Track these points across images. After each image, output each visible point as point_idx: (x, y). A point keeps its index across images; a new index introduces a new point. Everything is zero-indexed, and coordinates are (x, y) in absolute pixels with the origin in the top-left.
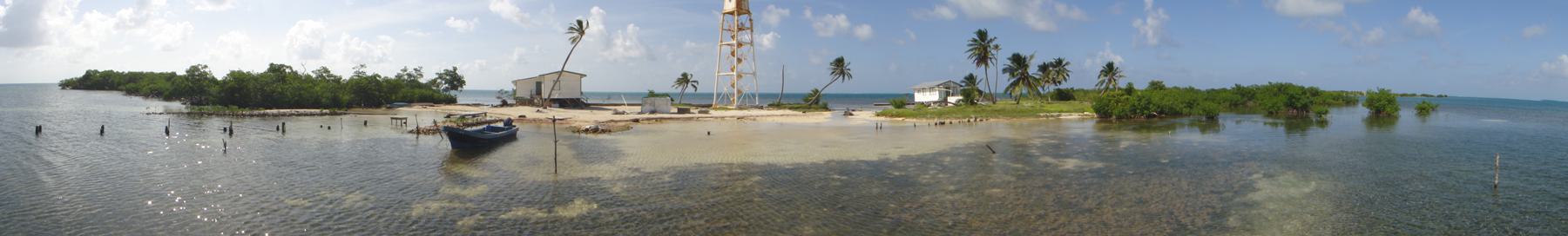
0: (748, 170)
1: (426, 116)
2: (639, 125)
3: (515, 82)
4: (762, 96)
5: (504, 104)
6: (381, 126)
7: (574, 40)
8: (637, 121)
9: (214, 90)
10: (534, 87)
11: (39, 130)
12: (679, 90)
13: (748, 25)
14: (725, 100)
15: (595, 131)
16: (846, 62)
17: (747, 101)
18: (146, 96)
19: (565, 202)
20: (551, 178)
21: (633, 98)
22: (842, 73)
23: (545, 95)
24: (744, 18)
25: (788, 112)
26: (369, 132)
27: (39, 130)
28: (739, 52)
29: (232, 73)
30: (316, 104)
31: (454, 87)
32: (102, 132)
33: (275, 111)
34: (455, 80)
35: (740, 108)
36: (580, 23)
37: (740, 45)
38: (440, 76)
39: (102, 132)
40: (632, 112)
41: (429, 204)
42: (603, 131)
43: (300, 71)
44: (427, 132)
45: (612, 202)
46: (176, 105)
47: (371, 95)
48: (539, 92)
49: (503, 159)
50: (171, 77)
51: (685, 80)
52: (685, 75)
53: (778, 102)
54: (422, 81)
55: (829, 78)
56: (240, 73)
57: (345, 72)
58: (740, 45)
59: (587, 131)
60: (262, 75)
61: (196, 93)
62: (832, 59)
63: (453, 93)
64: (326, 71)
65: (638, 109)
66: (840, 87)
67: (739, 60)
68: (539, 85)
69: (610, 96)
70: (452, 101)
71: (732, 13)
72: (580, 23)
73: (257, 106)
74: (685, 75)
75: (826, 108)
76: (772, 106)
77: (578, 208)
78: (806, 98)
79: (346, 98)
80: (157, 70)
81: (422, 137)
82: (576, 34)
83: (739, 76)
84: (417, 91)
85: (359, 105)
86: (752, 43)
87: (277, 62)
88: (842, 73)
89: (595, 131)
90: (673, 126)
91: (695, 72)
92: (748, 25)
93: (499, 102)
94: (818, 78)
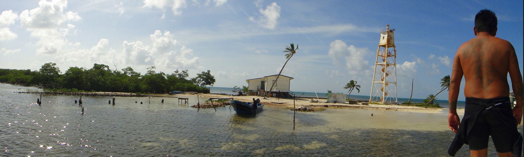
0: (402, 133)
1: (193, 99)
2: (328, 109)
3: (248, 81)
4: (399, 100)
5: (240, 94)
6: (172, 102)
7: (288, 57)
8: (327, 106)
9: (61, 79)
10: (259, 84)
11: (372, 115)
13: (393, 53)
14: (377, 100)
15: (305, 110)
17: (390, 101)
18: (13, 83)
19: (309, 142)
20: (292, 131)
21: (322, 96)
23: (267, 88)
26: (165, 107)
27: (372, 115)
28: (387, 69)
29: (72, 69)
30: (126, 90)
31: (209, 83)
32: (292, 50)
33: (102, 93)
34: (209, 79)
35: (386, 104)
36: (292, 46)
37: (388, 65)
38: (200, 76)
39: (292, 50)
40: (323, 102)
42: (310, 110)
43: (112, 69)
44: (204, 107)
45: (332, 143)
46: (33, 89)
47: (158, 85)
48: (263, 87)
49: (261, 119)
50: (28, 72)
51: (352, 85)
53: (408, 102)
54: (188, 79)
56: (76, 68)
57: (142, 70)
58: (388, 65)
59: (299, 110)
60: (87, 72)
61: (47, 81)
62: (443, 77)
63: (208, 86)
64: (130, 69)
65: (326, 100)
67: (387, 75)
68: (263, 83)
69: (303, 94)
70: (207, 91)
71: (384, 46)
72: (292, 46)
73: (89, 90)
75: (438, 106)
76: (404, 104)
77: (315, 145)
78: (425, 101)
79: (144, 87)
80: (19, 69)
81: (201, 110)
82: (289, 53)
84: (186, 84)
85: (152, 92)
87: (99, 63)
89: (305, 110)
90: (346, 110)
91: (359, 81)
92: (393, 53)
93: (237, 93)
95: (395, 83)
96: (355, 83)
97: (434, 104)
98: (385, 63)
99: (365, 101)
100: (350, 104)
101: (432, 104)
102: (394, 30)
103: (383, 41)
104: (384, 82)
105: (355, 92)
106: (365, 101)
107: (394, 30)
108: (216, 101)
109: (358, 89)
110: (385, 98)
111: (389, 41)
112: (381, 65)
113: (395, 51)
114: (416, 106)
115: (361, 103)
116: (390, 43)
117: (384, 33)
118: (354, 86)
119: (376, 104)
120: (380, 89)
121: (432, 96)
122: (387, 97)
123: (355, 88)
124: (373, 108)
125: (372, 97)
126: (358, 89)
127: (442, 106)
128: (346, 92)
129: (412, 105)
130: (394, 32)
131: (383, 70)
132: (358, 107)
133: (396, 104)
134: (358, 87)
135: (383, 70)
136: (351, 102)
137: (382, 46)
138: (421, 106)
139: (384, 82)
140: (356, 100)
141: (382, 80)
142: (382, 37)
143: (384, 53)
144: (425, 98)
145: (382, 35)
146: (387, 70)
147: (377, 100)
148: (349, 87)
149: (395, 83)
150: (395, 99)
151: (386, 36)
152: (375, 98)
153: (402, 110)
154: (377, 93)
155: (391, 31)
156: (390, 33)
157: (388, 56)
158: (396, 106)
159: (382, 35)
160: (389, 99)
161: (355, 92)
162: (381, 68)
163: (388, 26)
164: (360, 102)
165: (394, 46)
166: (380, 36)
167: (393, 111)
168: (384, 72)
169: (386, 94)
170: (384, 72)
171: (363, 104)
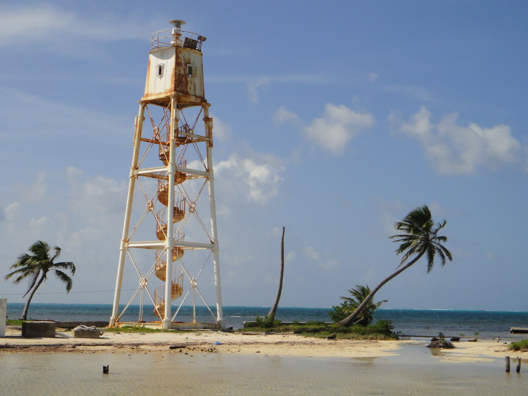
4: (228, 312)
11: (106, 370)
12: (252, 184)
13: (200, 130)
14: (140, 316)
16: (436, 218)
22: (428, 248)
24: (191, 115)
25: (300, 338)
27: (106, 370)
28: (180, 192)
37: (180, 176)
41: (248, 164)
51: (38, 260)
52: (40, 249)
53: (268, 322)
55: (396, 260)
62: (403, 214)
66: (415, 288)
67: (178, 213)
71: (163, 103)
74: (40, 249)
75: (387, 332)
78: (337, 314)
83: (177, 251)
86: (208, 173)
88: (428, 248)
91: (67, 246)
92: (200, 130)
94: (364, 257)
95: (213, 246)
96: (51, 254)
97: (374, 323)
98: (169, 169)
99: (93, 323)
100: (25, 336)
101: (364, 323)
102: (202, 39)
103: (160, 83)
104: (166, 243)
105: (51, 291)
106: (93, 323)
107: (202, 39)
108: (69, 347)
109: (65, 278)
110: (173, 310)
111: (181, 81)
112: (153, 176)
113: (207, 119)
114: (298, 332)
115: (71, 334)
116: (186, 90)
117: (162, 53)
118: (46, 266)
119: (136, 330)
120: (151, 272)
121: (363, 293)
122: (181, 302)
123: (51, 272)
124: (121, 346)
125: (120, 308)
126: (65, 278)
127: (404, 331)
128: (17, 292)
129: (284, 329)
130: (204, 47)
131: (163, 197)
132: (57, 347)
133: (217, 328)
134: (67, 271)
135: (163, 197)
136: (31, 330)
137: (155, 102)
138: (314, 332)
139: (166, 243)
140: (44, 319)
141: (161, 236)
142: (153, 70)
143: (164, 132)
144: (338, 303)
145: (154, 61)
146: (178, 197)
147: (140, 316)
148: (27, 271)
149: (213, 246)
150: (214, 310)
151: (170, 64)
152: (133, 311)
153: (234, 349)
154: (142, 289)
155: (191, 44)
156: (187, 53)
157: (181, 140)
158: (213, 337)
159: (154, 61)
160: (186, 311)
161: (51, 291)
162: (151, 187)
163: (178, 24)
164: (69, 327)
165: (203, 102)
166: (148, 63)
167: (198, 354)
168: (165, 203)
169: (176, 290)
170: (165, 203)
171: (78, 334)
